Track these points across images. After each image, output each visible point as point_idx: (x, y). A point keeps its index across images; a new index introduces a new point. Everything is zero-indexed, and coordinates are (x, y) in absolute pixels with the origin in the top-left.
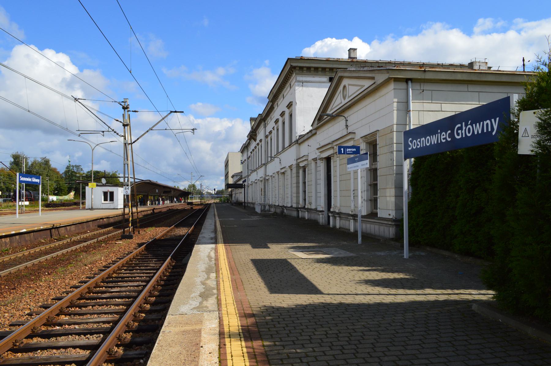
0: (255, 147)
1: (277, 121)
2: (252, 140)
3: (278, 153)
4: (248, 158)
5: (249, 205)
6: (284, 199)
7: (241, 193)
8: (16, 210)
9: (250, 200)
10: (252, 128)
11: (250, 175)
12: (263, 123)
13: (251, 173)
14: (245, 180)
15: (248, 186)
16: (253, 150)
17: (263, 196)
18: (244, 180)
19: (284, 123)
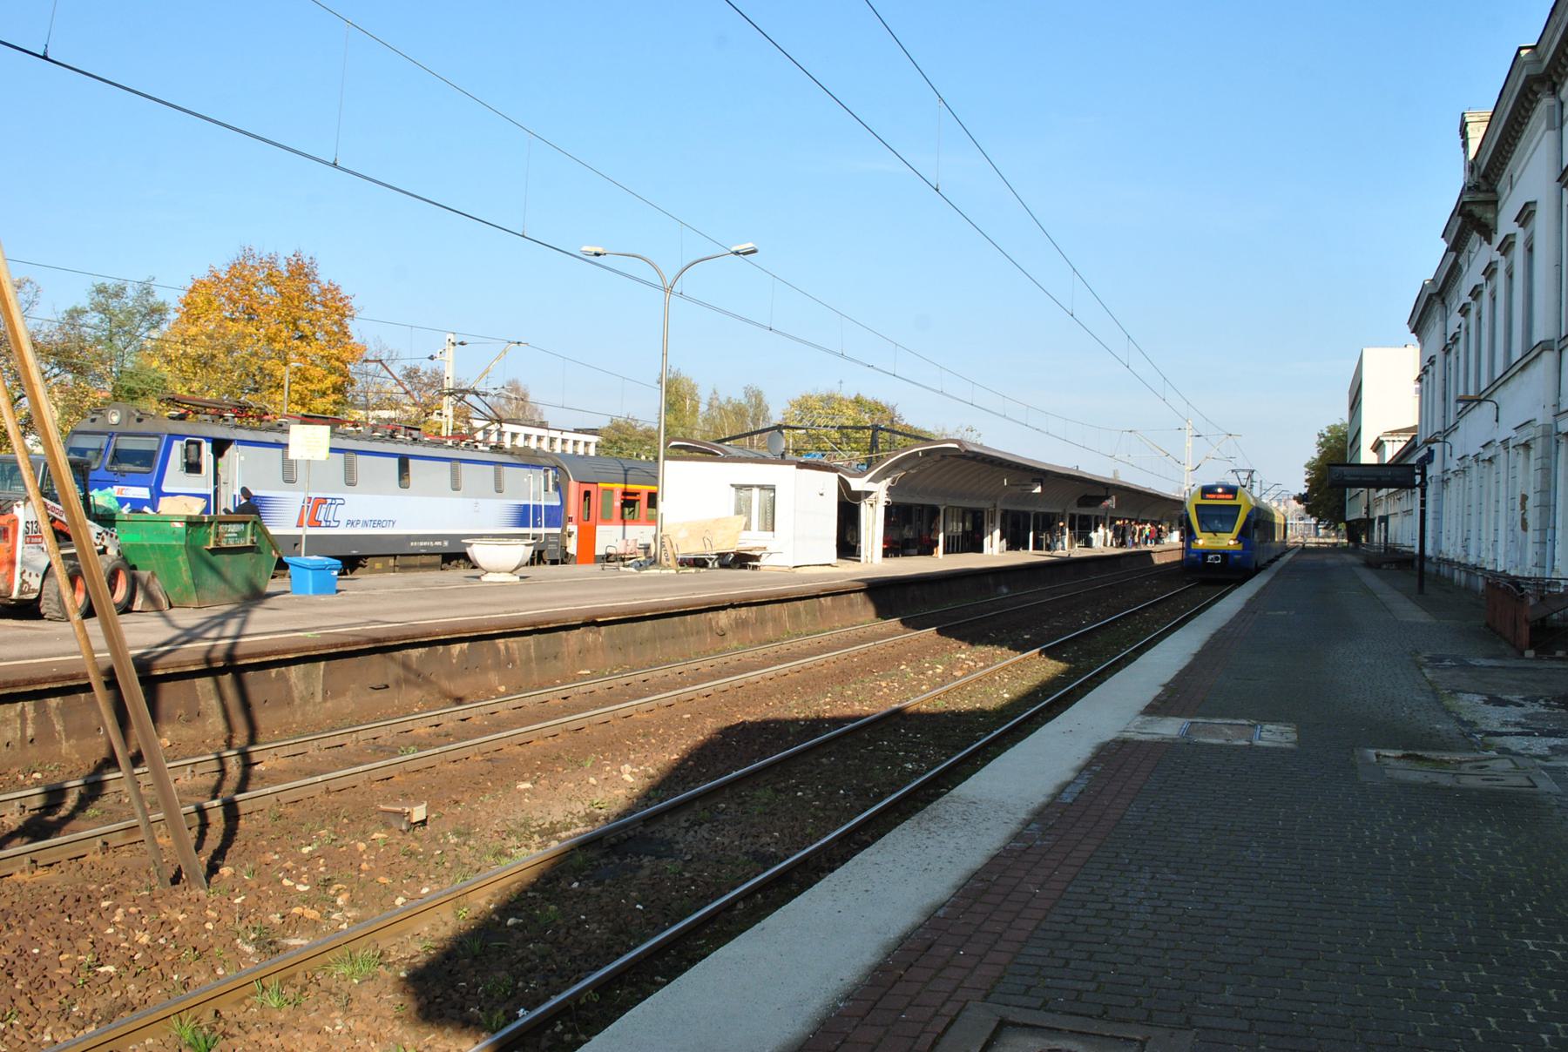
0: (1490, 271)
1: (1464, 311)
2: (1475, 236)
3: (1495, 385)
4: (1446, 350)
5: (1445, 570)
6: (1465, 548)
7: (1408, 512)
8: (535, 525)
9: (1452, 550)
10: (1472, 167)
11: (1455, 428)
12: (1545, 103)
13: (1460, 415)
14: (1431, 452)
15: (1445, 482)
16: (1476, 293)
17: (1532, 535)
18: (1424, 452)
19: (1510, 276)
